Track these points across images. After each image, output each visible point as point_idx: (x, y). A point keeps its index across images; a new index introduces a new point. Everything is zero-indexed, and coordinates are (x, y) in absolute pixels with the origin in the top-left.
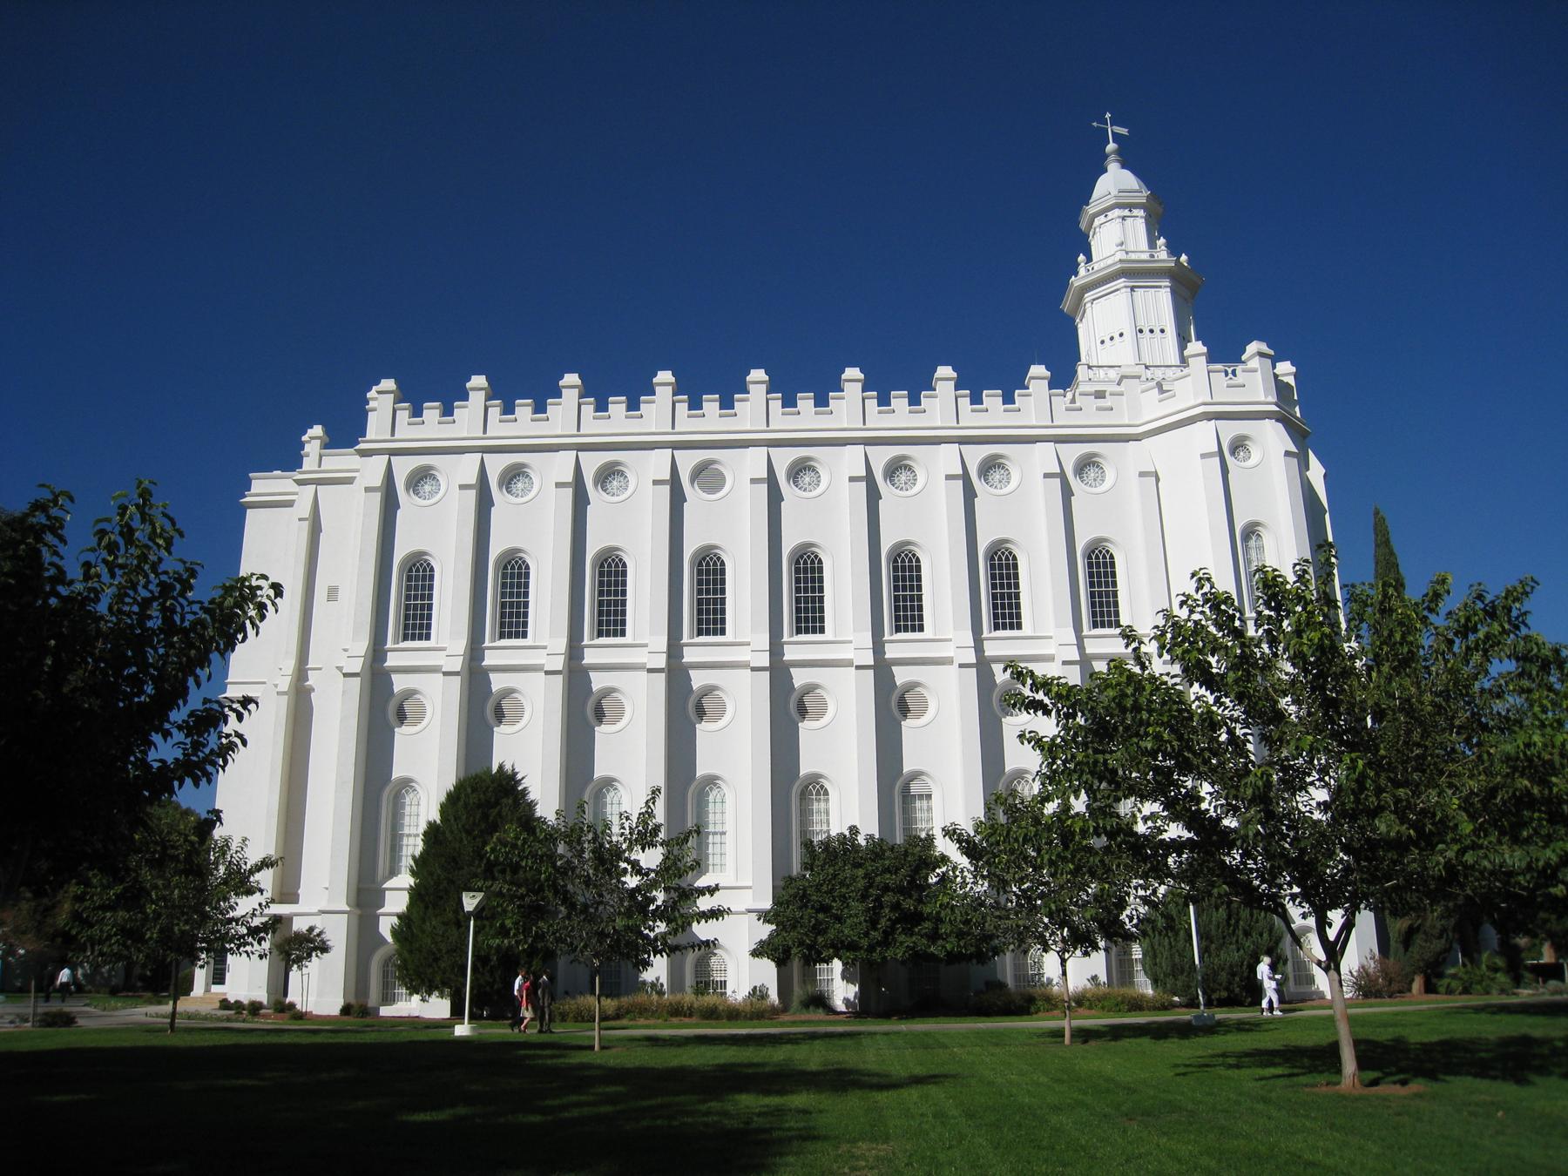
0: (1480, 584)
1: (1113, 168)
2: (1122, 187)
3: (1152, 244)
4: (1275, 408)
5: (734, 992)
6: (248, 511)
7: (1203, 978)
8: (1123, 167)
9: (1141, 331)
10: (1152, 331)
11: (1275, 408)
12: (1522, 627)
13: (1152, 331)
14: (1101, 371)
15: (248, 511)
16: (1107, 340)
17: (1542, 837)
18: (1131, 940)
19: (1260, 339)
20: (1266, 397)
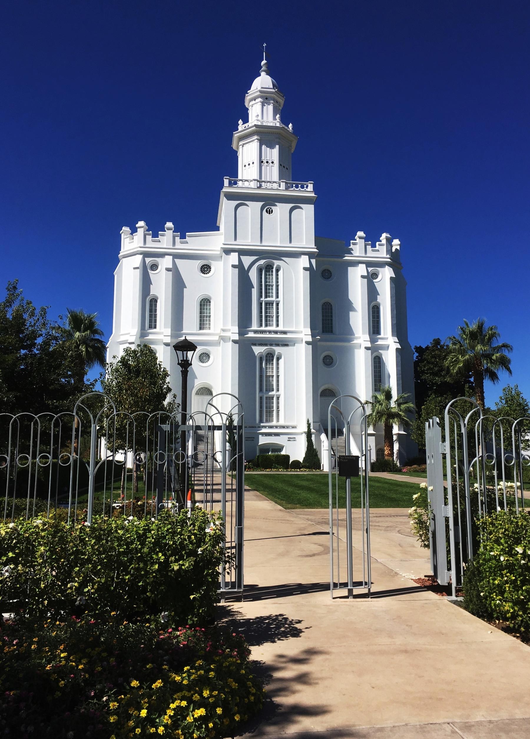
0: (492, 329)
1: (263, 74)
2: (264, 86)
3: (275, 119)
4: (389, 260)
5: (169, 383)
6: (350, 269)
7: (290, 503)
8: (267, 74)
9: (262, 162)
10: (267, 162)
11: (389, 260)
12: (497, 370)
13: (267, 162)
14: (246, 182)
15: (350, 269)
16: (247, 165)
17: (495, 519)
18: (311, 432)
19: (386, 232)
20: (387, 255)
